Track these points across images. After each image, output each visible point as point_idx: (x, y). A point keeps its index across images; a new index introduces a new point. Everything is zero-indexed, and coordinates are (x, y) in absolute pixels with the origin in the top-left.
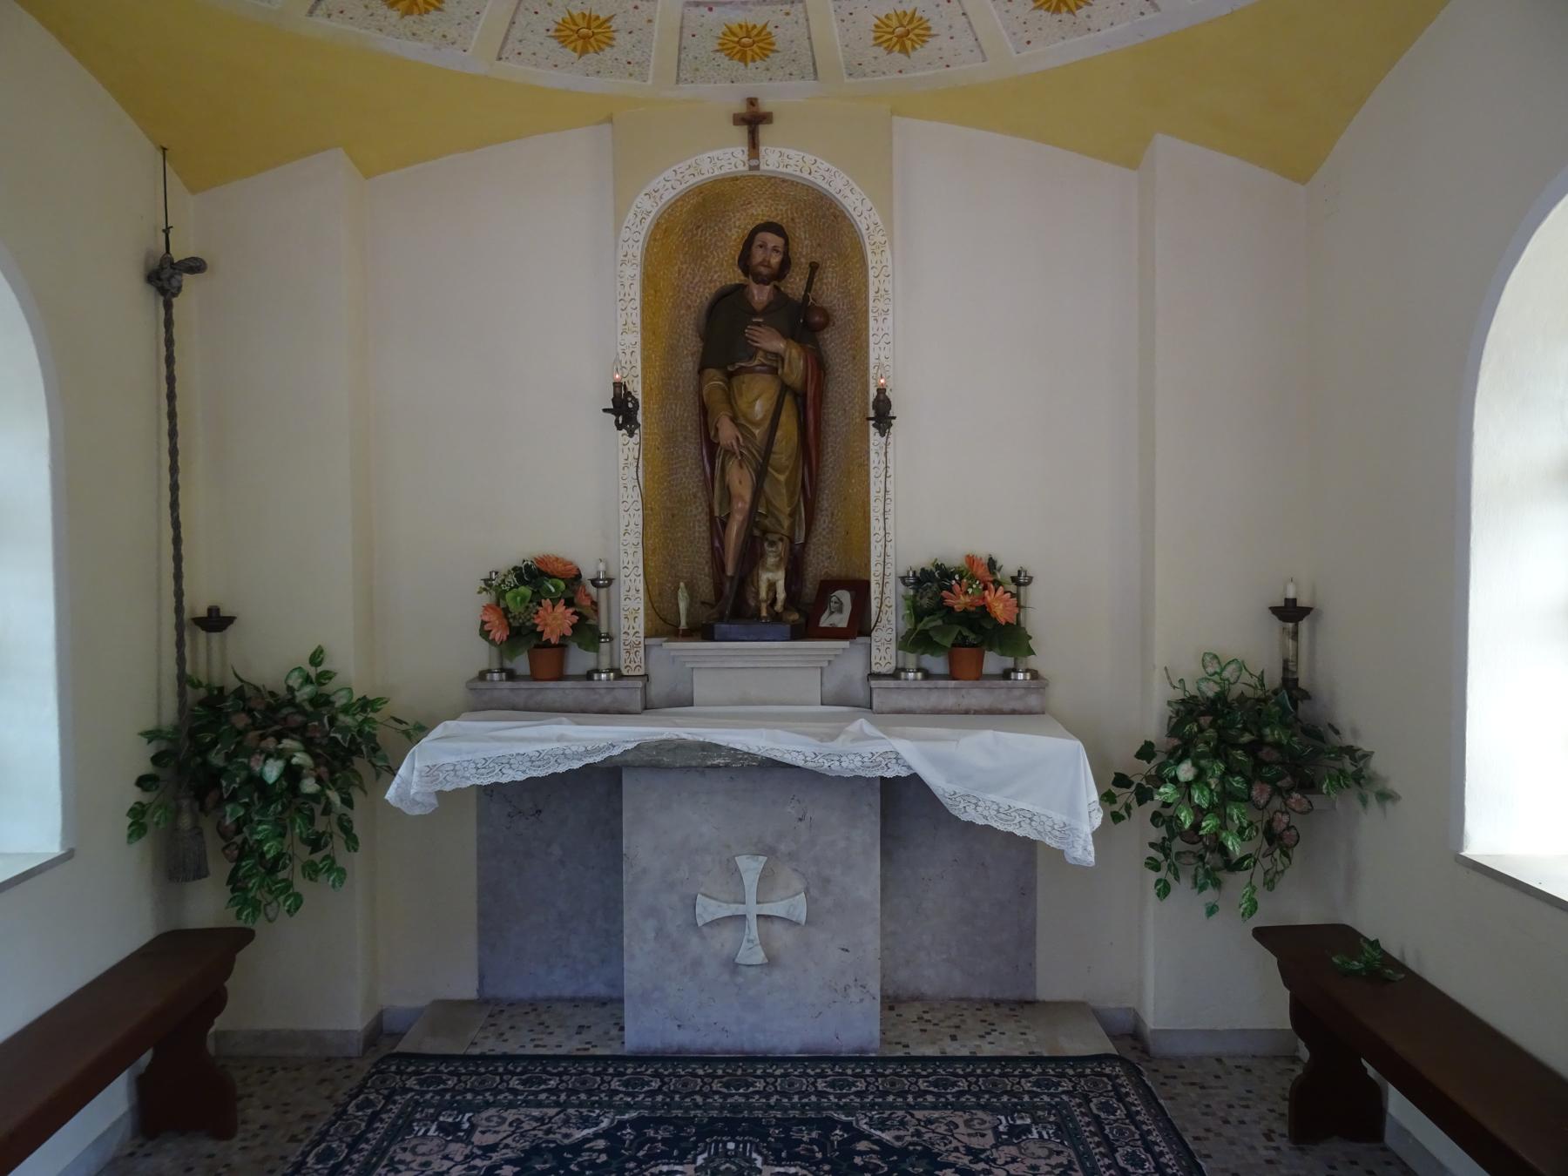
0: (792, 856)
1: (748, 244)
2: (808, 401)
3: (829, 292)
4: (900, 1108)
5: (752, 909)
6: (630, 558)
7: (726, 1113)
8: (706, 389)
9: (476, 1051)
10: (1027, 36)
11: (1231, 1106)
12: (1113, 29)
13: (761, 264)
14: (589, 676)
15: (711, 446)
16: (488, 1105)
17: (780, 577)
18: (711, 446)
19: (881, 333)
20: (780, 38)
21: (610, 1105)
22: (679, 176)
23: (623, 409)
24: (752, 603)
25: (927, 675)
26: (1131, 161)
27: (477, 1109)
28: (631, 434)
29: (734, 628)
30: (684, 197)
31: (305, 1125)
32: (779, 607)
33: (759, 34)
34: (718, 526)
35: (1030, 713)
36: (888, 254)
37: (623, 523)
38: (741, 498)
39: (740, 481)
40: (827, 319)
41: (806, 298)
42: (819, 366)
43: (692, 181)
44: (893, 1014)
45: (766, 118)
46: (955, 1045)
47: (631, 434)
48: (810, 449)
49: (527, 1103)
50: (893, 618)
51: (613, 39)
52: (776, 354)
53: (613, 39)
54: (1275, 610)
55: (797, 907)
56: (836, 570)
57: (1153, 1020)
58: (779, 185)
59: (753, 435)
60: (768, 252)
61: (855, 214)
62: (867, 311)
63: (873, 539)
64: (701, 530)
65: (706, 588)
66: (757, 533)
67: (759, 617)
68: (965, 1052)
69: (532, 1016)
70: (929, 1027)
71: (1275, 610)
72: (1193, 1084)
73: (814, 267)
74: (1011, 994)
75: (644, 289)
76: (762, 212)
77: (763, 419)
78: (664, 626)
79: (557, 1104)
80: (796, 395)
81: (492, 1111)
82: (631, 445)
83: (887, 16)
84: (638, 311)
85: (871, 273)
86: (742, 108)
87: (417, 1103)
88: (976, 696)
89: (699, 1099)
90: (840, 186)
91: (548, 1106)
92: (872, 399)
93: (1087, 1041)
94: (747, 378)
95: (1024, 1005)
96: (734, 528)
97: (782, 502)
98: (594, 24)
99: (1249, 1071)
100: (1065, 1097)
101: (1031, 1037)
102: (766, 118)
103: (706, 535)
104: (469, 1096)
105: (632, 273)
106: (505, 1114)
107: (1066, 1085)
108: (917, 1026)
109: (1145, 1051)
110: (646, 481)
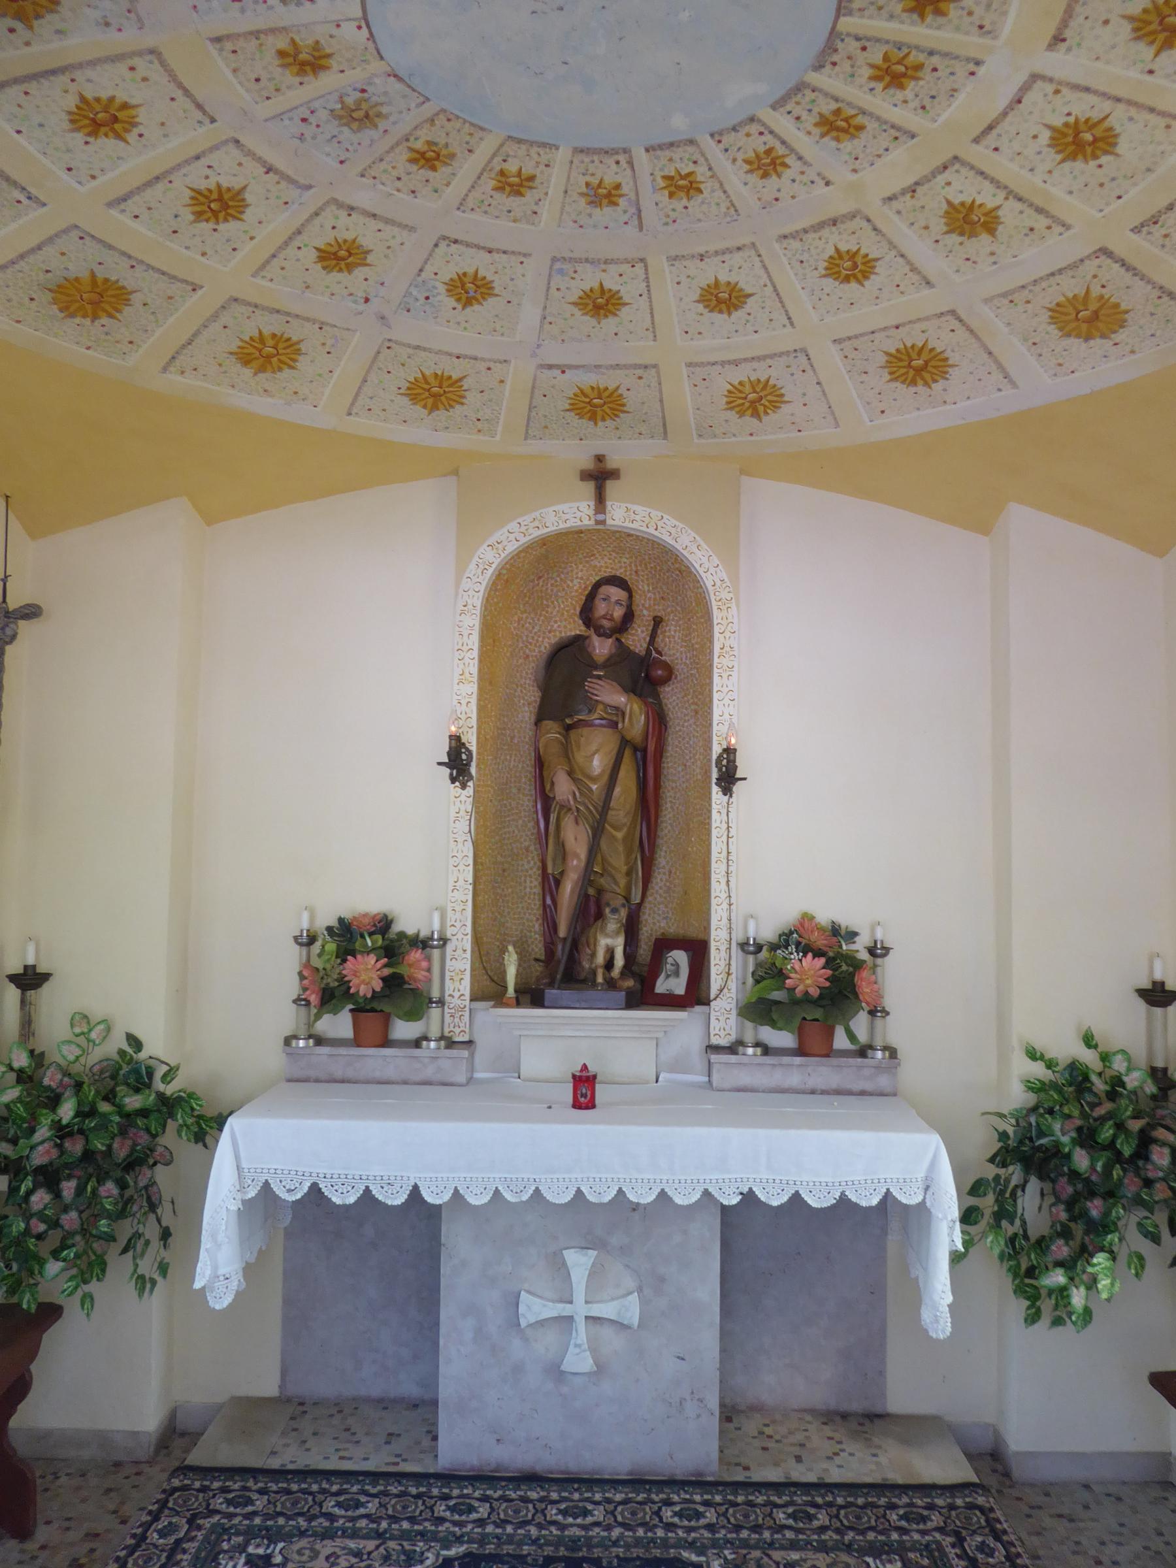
0: (624, 1251)
1: (591, 597)
2: (646, 757)
3: (672, 647)
4: (756, 1547)
5: (580, 1309)
6: (458, 915)
7: (562, 1552)
8: (543, 741)
9: (275, 1463)
10: (882, 407)
11: (1103, 1543)
12: (969, 402)
13: (604, 617)
14: (417, 1044)
15: (546, 800)
16: (302, 1534)
17: (619, 944)
18: (546, 800)
19: (725, 690)
20: (632, 400)
21: (434, 1537)
22: (523, 529)
23: (457, 762)
24: (586, 965)
25: (767, 1050)
26: (984, 528)
27: (287, 1537)
28: (464, 786)
29: (566, 995)
30: (527, 549)
31: (87, 1546)
32: (616, 972)
33: (610, 395)
34: (551, 884)
35: (882, 1094)
36: (733, 606)
37: (452, 879)
38: (577, 856)
39: (576, 838)
40: (669, 673)
41: (648, 650)
42: (659, 720)
43: (536, 533)
44: (731, 1426)
45: (614, 474)
46: (801, 1468)
47: (464, 786)
48: (648, 804)
49: (345, 1534)
50: (734, 990)
51: (464, 397)
52: (617, 708)
53: (464, 397)
54: (1143, 993)
55: (630, 1309)
56: (672, 928)
57: (1020, 1439)
58: (624, 540)
59: (590, 790)
60: (610, 605)
61: (701, 571)
62: (711, 666)
63: (714, 902)
64: (533, 885)
65: (538, 950)
66: (591, 891)
67: (594, 984)
68: (811, 1478)
69: (336, 1421)
70: (771, 1444)
71: (1143, 993)
72: (1060, 1516)
73: (657, 622)
74: (856, 1406)
75: (483, 638)
76: (606, 565)
77: (601, 775)
78: (489, 991)
79: (379, 1535)
80: (635, 749)
81: (303, 1543)
82: (463, 798)
83: (741, 383)
84: (476, 661)
85: (716, 629)
86: (588, 464)
87: (225, 1530)
88: (821, 1073)
89: (534, 1531)
90: (687, 542)
91: (366, 1537)
92: (714, 757)
93: (942, 1466)
94: (585, 731)
95: (867, 1421)
96: (568, 889)
97: (617, 859)
98: (445, 384)
99: (1119, 1499)
100: (938, 1536)
101: (883, 1459)
102: (614, 474)
103: (538, 890)
104: (281, 1521)
105: (472, 622)
106: (318, 1547)
107: (936, 1520)
108: (757, 1443)
109: (1007, 1474)
110: (477, 833)
